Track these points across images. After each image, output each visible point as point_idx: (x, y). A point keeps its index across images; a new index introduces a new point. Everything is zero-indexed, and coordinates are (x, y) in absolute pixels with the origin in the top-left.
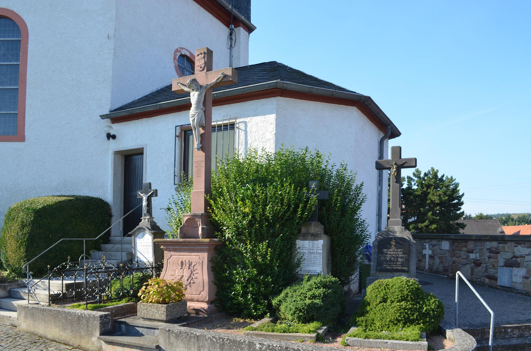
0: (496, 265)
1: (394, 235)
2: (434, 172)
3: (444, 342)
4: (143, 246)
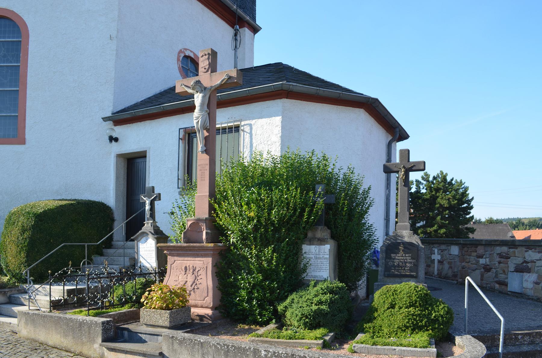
0: (506, 270)
1: (402, 240)
2: (443, 176)
3: (453, 349)
4: (146, 251)
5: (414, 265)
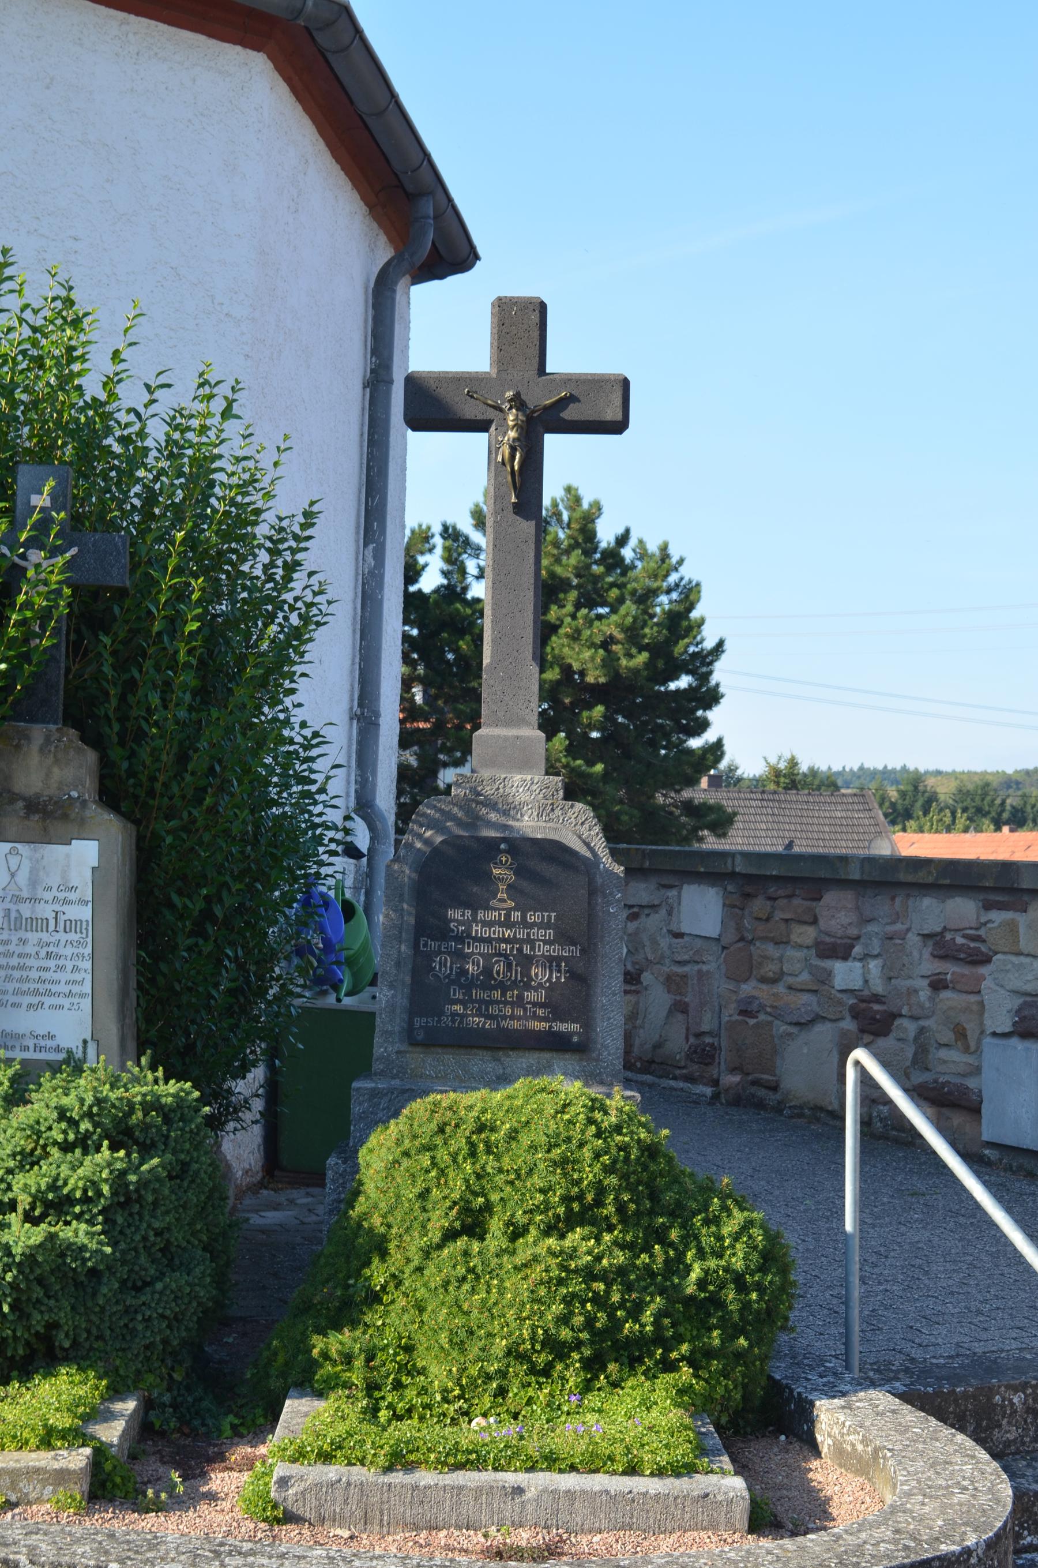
0: (971, 1028)
1: (505, 827)
2: (577, 515)
3: (810, 1475)
5: (574, 976)
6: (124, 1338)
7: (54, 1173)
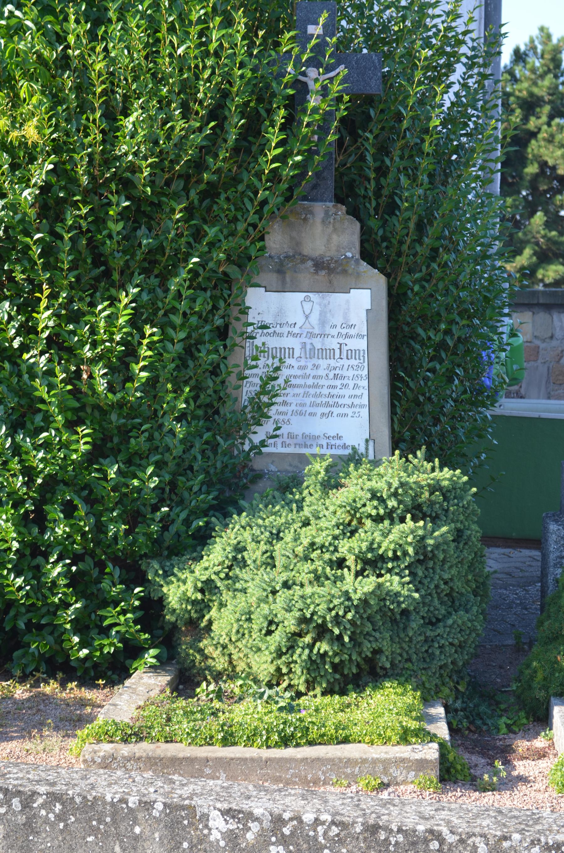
2: (549, 48)
6: (425, 661)
7: (370, 538)
